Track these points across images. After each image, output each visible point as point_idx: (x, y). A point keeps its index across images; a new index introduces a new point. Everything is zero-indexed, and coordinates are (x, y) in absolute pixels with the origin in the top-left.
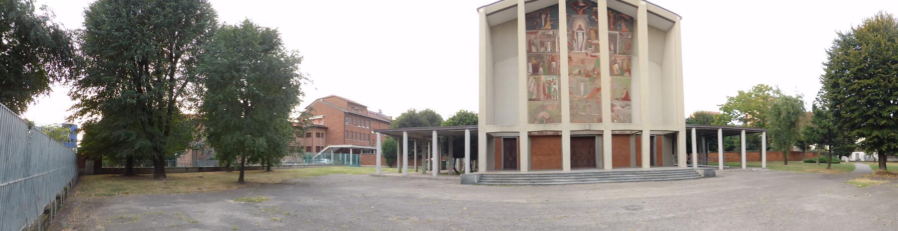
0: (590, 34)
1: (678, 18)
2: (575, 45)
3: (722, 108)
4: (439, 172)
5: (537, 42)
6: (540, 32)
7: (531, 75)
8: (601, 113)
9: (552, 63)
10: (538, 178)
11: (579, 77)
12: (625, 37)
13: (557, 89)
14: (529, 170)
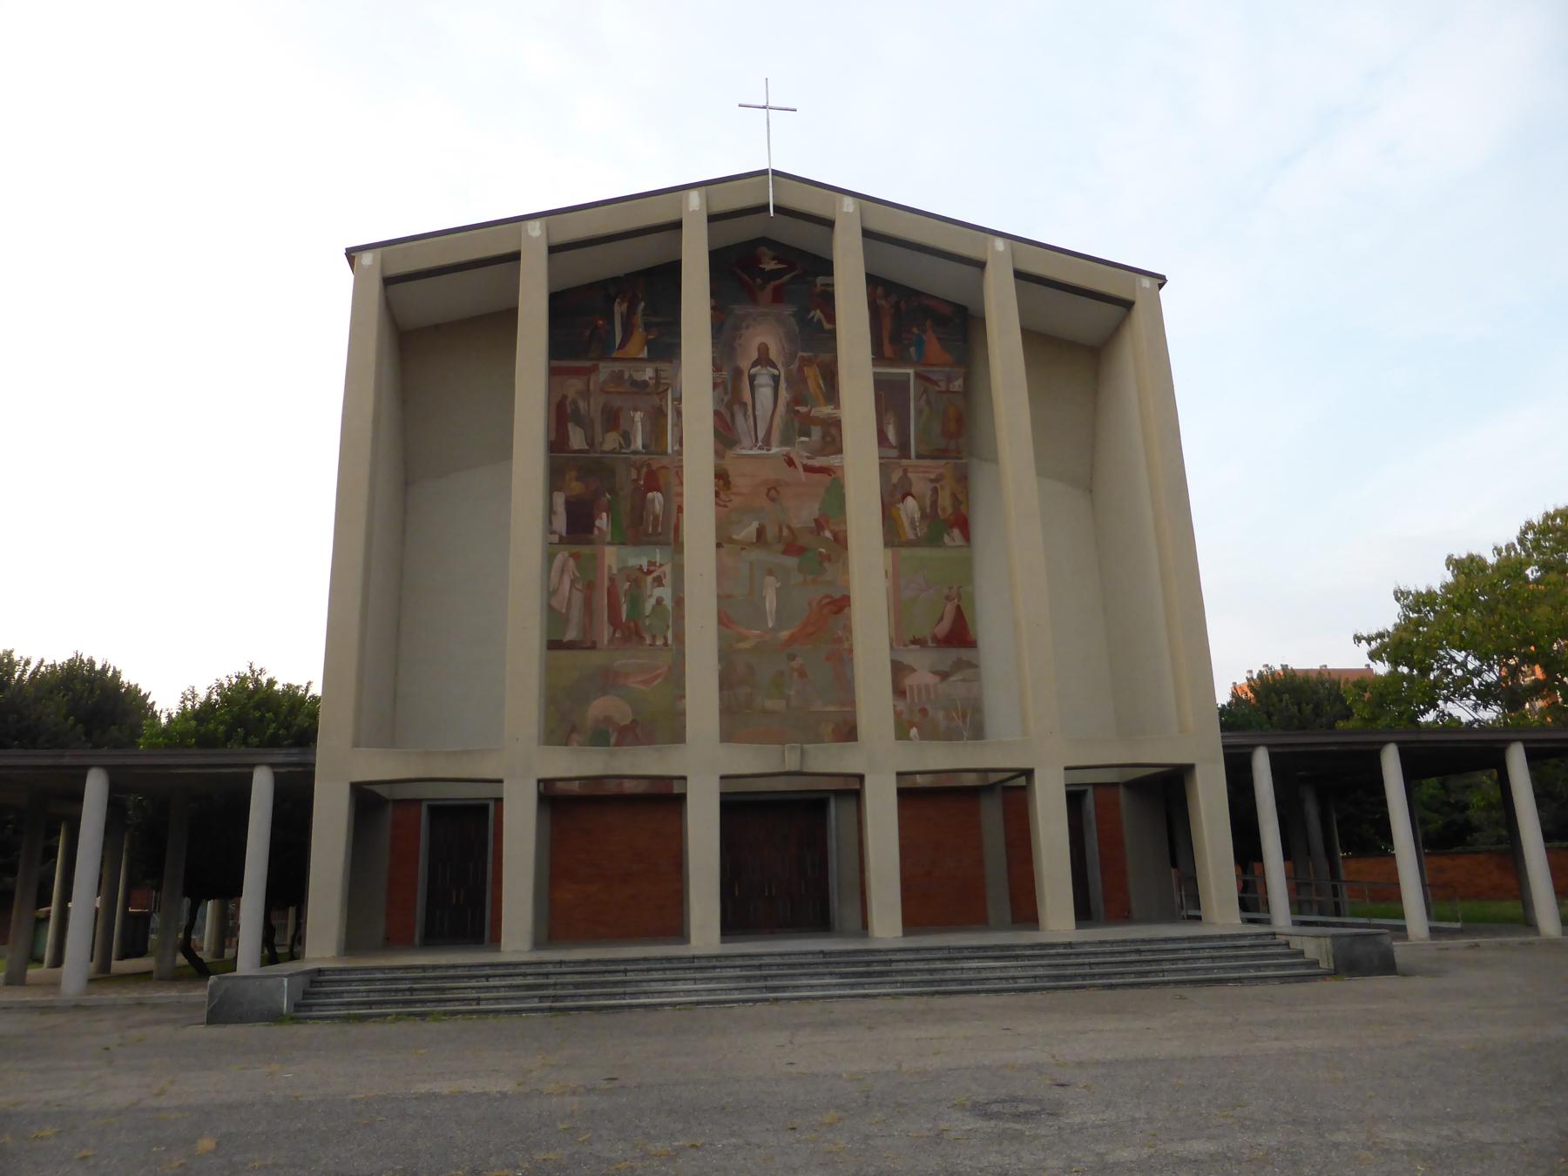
0: (804, 380)
1: (1146, 282)
2: (742, 424)
3: (1383, 648)
4: (105, 966)
5: (593, 408)
6: (605, 370)
7: (562, 541)
8: (853, 703)
9: (650, 495)
10: (578, 978)
11: (755, 555)
12: (943, 386)
13: (668, 603)
14: (538, 945)
